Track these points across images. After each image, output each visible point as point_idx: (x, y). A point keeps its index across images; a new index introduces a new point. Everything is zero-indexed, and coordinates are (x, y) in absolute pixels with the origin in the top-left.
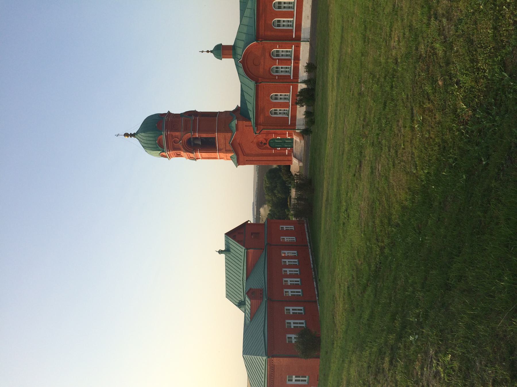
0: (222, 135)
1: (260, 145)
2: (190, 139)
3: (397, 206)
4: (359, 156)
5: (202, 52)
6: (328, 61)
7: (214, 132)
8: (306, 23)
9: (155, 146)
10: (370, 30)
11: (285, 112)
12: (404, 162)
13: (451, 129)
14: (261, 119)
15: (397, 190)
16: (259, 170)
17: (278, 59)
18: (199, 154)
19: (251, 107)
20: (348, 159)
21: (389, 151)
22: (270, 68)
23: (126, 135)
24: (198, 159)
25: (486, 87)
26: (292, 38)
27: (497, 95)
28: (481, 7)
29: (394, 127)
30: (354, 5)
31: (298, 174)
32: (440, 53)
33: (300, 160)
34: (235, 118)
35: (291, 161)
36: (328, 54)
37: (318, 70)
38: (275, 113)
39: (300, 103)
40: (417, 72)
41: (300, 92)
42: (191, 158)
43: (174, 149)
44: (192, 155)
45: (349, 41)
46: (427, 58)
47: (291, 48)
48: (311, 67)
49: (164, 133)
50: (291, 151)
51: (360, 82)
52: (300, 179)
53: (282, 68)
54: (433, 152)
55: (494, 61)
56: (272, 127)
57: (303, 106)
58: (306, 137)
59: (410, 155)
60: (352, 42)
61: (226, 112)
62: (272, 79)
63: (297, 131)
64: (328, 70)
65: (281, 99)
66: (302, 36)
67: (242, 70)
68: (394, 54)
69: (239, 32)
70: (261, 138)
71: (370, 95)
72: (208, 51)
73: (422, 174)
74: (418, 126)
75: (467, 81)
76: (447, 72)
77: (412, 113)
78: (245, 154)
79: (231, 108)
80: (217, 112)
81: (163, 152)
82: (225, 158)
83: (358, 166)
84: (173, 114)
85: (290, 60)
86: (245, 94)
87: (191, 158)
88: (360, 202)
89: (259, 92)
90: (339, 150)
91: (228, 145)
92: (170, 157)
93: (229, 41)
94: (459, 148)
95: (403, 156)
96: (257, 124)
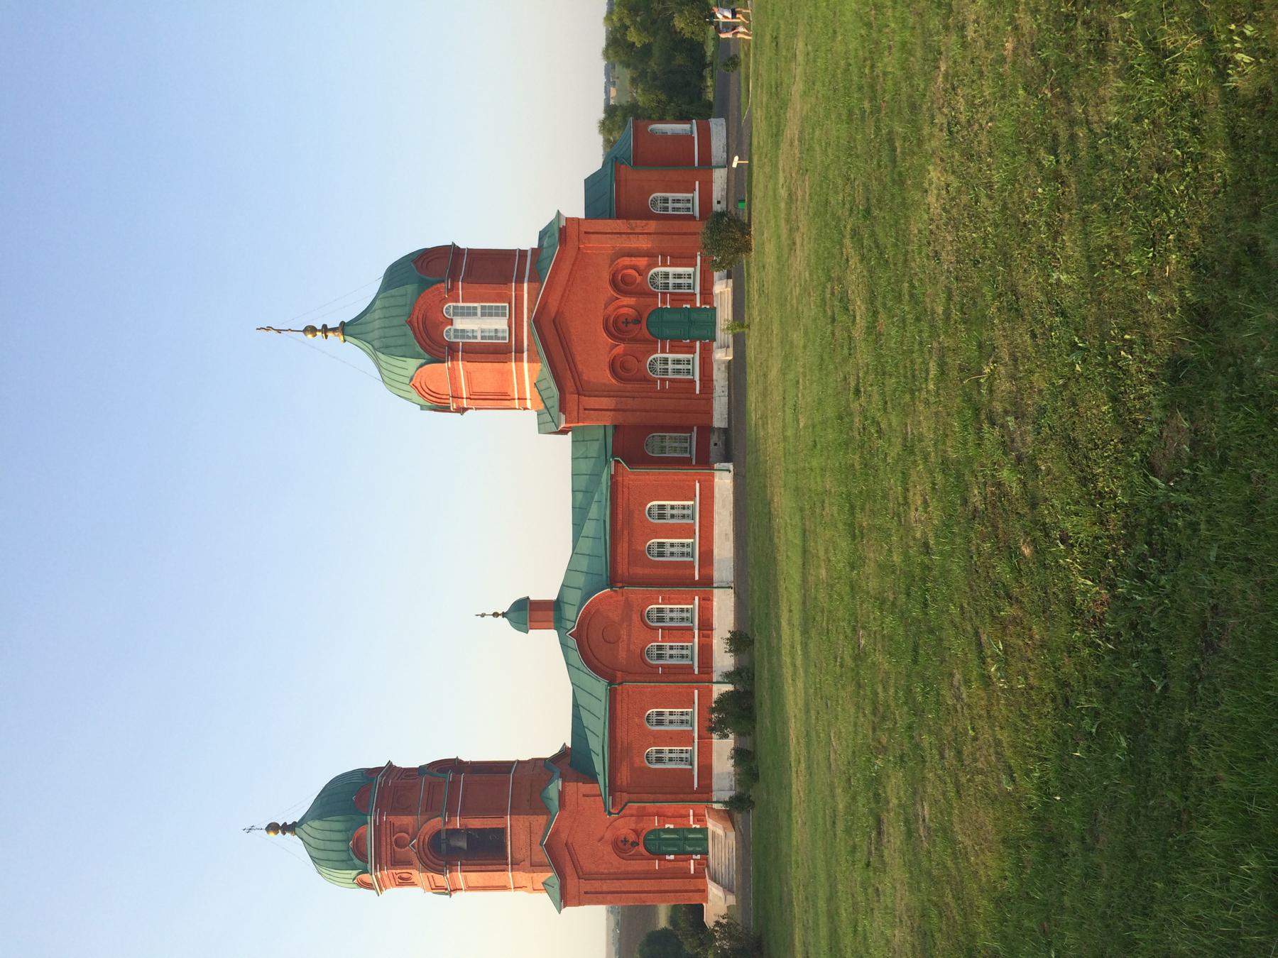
0: (523, 821)
1: (621, 847)
2: (439, 832)
3: (984, 904)
4: (873, 805)
5: (483, 615)
6: (778, 617)
7: (502, 813)
8: (724, 549)
9: (344, 856)
10: (863, 509)
11: (684, 755)
12: (981, 772)
13: (1071, 649)
14: (624, 776)
15: (977, 856)
16: (620, 939)
17: (662, 628)
18: (459, 877)
19: (597, 744)
20: (848, 831)
21: (942, 757)
22: (642, 649)
23: (273, 828)
24: (456, 890)
25: (1125, 527)
26: (691, 580)
27: (1150, 533)
28: (1078, 368)
29: (943, 692)
30: (822, 476)
31: (724, 921)
32: (1015, 489)
33: (728, 889)
34: (557, 774)
35: (703, 891)
36: (777, 602)
37: (757, 645)
38: (659, 760)
39: (719, 727)
40: (973, 548)
41: (719, 701)
42: (438, 888)
43: (396, 862)
44: (440, 880)
45: (821, 553)
46: (990, 510)
47: (692, 603)
48: (739, 642)
49: (371, 819)
50: (703, 863)
51: (854, 630)
52: (730, 937)
53: (671, 648)
54: (1044, 719)
55: (1128, 465)
56: (652, 797)
57: (726, 736)
58: (738, 817)
59: (992, 750)
60: (827, 551)
61: (535, 761)
62: (650, 674)
63: (716, 806)
64: (780, 637)
65: (671, 722)
66: (716, 576)
67: (576, 656)
68: (918, 535)
69: (574, 459)
70: (625, 827)
71: (879, 646)
72: (496, 615)
73: (1028, 787)
74: (998, 669)
75: (1080, 526)
76: (1036, 522)
77: (979, 644)
78: (583, 875)
79: (548, 749)
80: (513, 763)
81: (365, 871)
82: (530, 886)
83: (874, 834)
84: (400, 769)
85: (691, 629)
86: (583, 713)
87: (438, 888)
88: (888, 932)
89: (618, 706)
90: (824, 818)
91: (537, 848)
92: (382, 886)
93: (547, 590)
94: (1098, 683)
95: (975, 760)
96: (613, 788)
